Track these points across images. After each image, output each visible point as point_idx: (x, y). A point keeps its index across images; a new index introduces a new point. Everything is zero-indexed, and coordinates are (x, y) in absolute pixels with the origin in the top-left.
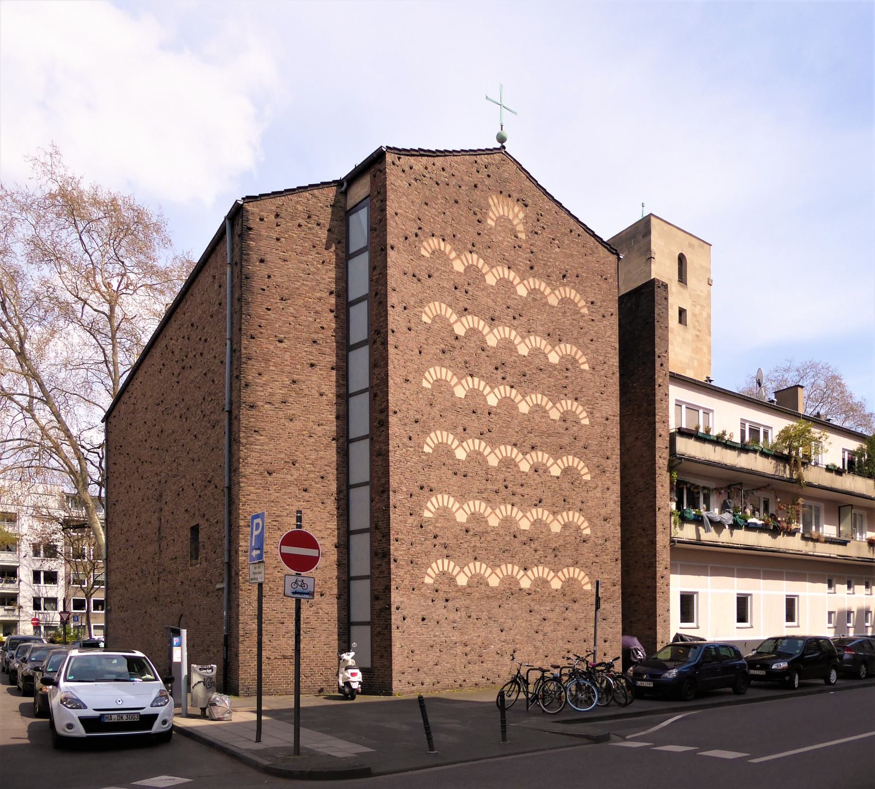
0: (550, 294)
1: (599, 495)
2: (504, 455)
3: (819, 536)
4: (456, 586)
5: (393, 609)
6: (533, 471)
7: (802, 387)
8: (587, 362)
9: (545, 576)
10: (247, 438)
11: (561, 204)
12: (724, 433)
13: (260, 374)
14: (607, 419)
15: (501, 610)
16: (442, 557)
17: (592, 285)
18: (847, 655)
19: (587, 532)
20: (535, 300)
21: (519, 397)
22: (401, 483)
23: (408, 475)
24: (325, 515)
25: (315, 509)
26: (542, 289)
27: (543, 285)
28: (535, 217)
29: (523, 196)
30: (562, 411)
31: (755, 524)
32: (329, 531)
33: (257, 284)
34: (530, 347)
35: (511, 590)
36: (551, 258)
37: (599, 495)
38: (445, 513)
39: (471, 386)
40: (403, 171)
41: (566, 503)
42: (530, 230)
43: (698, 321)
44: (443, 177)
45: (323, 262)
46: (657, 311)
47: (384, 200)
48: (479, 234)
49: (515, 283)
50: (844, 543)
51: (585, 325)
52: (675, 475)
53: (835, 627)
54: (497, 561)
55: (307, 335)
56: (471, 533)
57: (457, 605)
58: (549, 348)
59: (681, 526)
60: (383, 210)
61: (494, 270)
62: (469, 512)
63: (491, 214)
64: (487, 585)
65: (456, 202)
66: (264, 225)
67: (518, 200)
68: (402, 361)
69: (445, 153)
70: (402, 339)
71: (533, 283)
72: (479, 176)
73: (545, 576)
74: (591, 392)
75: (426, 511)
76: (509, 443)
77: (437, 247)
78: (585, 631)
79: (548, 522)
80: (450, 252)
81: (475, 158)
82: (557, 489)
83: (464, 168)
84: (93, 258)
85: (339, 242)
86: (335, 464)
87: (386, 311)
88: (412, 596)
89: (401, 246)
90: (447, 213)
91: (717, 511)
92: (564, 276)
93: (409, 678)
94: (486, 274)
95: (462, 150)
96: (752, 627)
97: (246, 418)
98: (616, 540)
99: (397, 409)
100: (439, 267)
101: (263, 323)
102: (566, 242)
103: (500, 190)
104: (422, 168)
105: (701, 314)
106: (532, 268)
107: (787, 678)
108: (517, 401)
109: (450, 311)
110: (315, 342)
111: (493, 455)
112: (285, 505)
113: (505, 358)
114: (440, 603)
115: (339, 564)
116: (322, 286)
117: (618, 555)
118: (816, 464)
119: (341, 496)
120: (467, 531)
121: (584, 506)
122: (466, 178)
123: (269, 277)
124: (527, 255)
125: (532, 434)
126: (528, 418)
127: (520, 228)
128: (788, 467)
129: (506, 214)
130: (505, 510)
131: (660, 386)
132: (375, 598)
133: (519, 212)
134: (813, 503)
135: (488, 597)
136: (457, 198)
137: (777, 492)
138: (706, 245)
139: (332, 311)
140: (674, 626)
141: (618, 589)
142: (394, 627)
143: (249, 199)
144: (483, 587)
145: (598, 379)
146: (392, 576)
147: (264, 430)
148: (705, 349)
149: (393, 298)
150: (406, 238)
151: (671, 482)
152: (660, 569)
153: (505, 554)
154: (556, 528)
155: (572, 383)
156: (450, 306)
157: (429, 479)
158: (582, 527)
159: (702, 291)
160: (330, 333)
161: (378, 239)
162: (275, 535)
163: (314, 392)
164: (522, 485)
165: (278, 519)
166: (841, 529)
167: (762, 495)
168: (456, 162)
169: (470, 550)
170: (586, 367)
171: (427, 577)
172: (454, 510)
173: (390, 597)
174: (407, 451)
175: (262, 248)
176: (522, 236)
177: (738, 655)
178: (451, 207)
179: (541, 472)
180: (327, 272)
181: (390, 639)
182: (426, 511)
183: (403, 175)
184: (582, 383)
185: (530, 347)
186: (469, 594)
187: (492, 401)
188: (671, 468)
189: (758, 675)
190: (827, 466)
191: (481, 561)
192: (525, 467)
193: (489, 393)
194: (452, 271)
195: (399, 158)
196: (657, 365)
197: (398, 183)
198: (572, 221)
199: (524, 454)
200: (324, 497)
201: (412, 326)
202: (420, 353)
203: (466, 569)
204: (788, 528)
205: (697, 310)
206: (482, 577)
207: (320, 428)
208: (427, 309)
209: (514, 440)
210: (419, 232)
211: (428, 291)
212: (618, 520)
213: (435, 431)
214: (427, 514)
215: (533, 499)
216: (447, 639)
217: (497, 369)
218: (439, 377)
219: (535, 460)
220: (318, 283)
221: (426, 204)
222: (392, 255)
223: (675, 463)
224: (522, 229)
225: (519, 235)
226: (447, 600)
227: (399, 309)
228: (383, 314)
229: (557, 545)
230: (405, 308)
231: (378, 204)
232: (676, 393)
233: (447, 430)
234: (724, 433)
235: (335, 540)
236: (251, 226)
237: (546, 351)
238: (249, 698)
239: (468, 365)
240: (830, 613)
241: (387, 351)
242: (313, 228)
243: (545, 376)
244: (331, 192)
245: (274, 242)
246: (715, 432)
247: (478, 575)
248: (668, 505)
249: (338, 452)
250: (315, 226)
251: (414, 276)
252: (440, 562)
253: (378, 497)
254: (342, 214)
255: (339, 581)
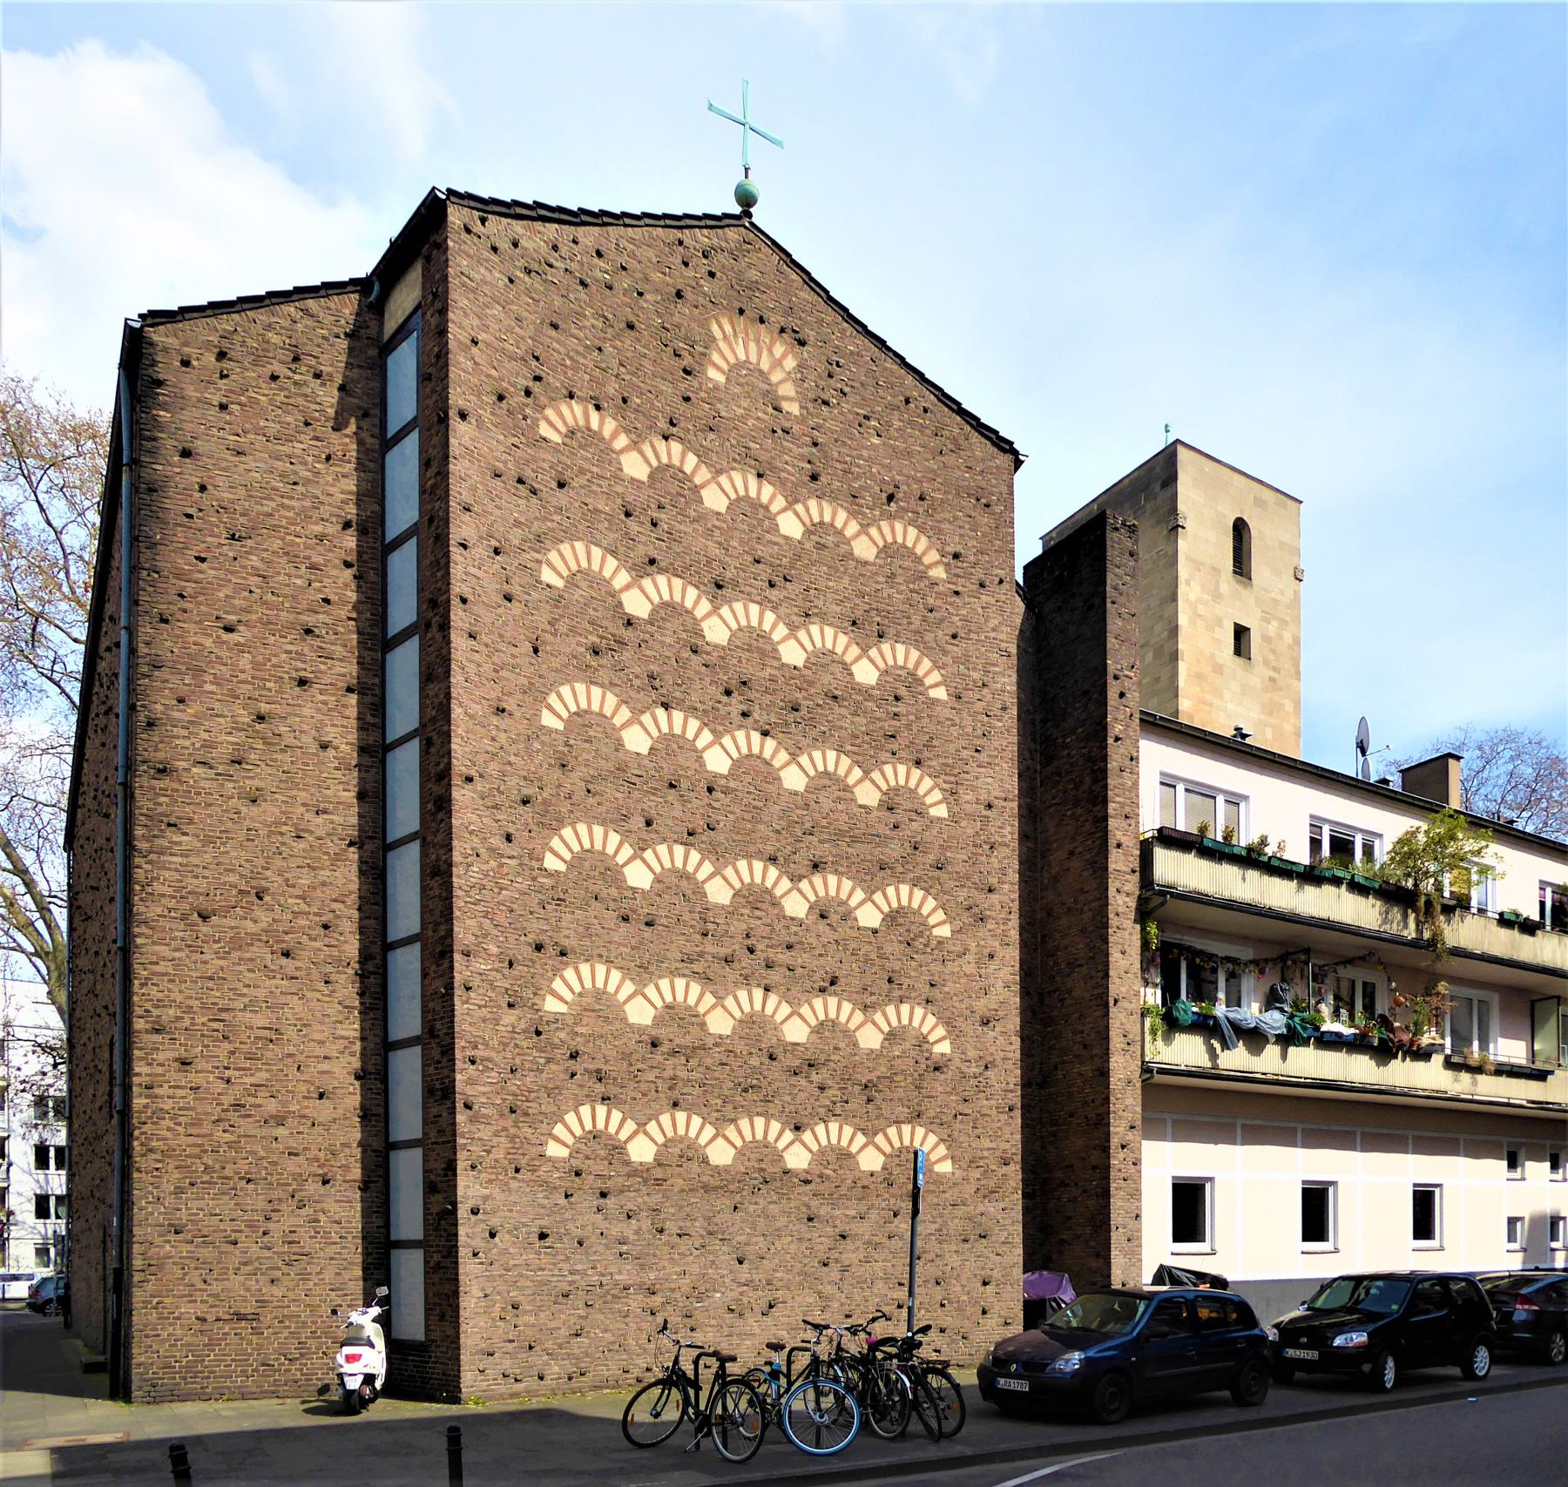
0: (857, 535)
1: (970, 969)
2: (747, 880)
3: (1484, 1061)
4: (628, 1163)
5: (463, 1212)
6: (814, 917)
7: (1458, 758)
8: (944, 683)
9: (844, 1143)
10: (150, 838)
11: (883, 342)
12: (1264, 842)
13: (181, 701)
14: (990, 806)
15: (738, 1216)
16: (590, 1099)
17: (956, 518)
18: (1521, 1312)
19: (944, 1048)
20: (821, 546)
21: (783, 756)
22: (485, 936)
23: (502, 918)
24: (333, 1010)
25: (309, 995)
26: (839, 524)
27: (842, 516)
28: (822, 368)
29: (794, 323)
30: (884, 787)
31: (1338, 1035)
32: (341, 1044)
33: (173, 505)
34: (810, 648)
35: (762, 1171)
36: (860, 457)
37: (970, 969)
38: (597, 1005)
39: (665, 729)
40: (495, 249)
41: (894, 986)
42: (811, 395)
43: (1273, 651)
44: (600, 271)
45: (328, 458)
46: (1110, 579)
47: (443, 311)
48: (687, 399)
49: (774, 508)
50: (1541, 1076)
51: (939, 603)
52: (1153, 929)
53: (1524, 1250)
54: (729, 1111)
55: (291, 617)
56: (664, 1048)
57: (630, 1206)
58: (855, 651)
59: (1168, 1038)
60: (442, 332)
61: (723, 479)
62: (659, 1004)
63: (716, 357)
64: (705, 1161)
65: (631, 326)
66: (190, 375)
67: (782, 330)
68: (487, 668)
69: (603, 218)
70: (487, 617)
71: (817, 510)
72: (689, 273)
73: (844, 1143)
74: (952, 748)
75: (549, 998)
76: (758, 855)
77: (582, 423)
78: (938, 1262)
79: (852, 1026)
80: (615, 435)
81: (678, 234)
82: (873, 956)
83: (651, 254)
84: (64, 538)
85: (366, 415)
86: (354, 897)
87: (447, 555)
88: (514, 1185)
89: (486, 415)
90: (608, 348)
91: (1255, 1007)
92: (891, 498)
93: (506, 1364)
94: (703, 486)
95: (646, 215)
96: (1336, 1251)
97: (150, 796)
98: (1009, 1065)
99: (473, 773)
100: (586, 466)
101: (190, 588)
102: (897, 424)
103: (737, 305)
104: (545, 249)
105: (1280, 637)
106: (814, 477)
107: (1367, 1368)
108: (777, 763)
109: (612, 563)
110: (308, 631)
111: (718, 880)
112: (239, 985)
113: (750, 670)
114: (586, 1201)
115: (366, 1115)
116: (325, 511)
117: (1016, 1099)
118: (1482, 911)
119: (370, 967)
120: (654, 1045)
121: (936, 993)
122: (656, 276)
123: (203, 488)
124: (805, 450)
125: (815, 837)
126: (805, 800)
127: (787, 390)
128: (1412, 917)
129: (753, 359)
130: (749, 1000)
131: (1117, 739)
132: (430, 1188)
133: (784, 356)
134: (1474, 994)
135: (706, 1188)
136: (632, 318)
137: (1391, 969)
138: (1290, 502)
139: (348, 565)
140: (1148, 1249)
141: (1014, 1172)
142: (464, 1252)
143: (155, 317)
144: (695, 1167)
145: (968, 721)
146: (460, 1141)
147: (191, 821)
148: (1289, 706)
149: (461, 528)
150: (501, 398)
151: (1145, 944)
152: (1118, 1130)
153: (751, 1095)
154: (870, 1039)
155: (909, 727)
156: (614, 553)
157: (558, 929)
158: (931, 1039)
159: (1282, 593)
160: (344, 612)
161: (435, 397)
162: (217, 1051)
163: (307, 740)
164: (789, 947)
165: (224, 1016)
166: (1536, 1047)
167: (1359, 975)
168: (632, 240)
169: (661, 1086)
170: (940, 693)
171: (551, 1143)
172: (779, 1018)
173: (455, 1186)
174: (501, 865)
175: (186, 426)
176: (793, 408)
177: (1245, 1313)
178: (617, 336)
179: (834, 918)
180: (337, 479)
181: (455, 1280)
182: (549, 998)
183: (493, 257)
184: (932, 728)
185: (810, 648)
186: (659, 1182)
187: (717, 763)
188: (1144, 914)
189: (1304, 1360)
190: (1501, 914)
191: (690, 1110)
192: (796, 907)
193: (711, 745)
194: (618, 475)
195: (483, 220)
196: (1112, 694)
197: (480, 273)
198: (909, 380)
199: (795, 878)
200: (329, 969)
201: (516, 590)
202: (536, 651)
203: (652, 1127)
204: (1412, 1042)
205: (1272, 628)
206: (692, 1145)
207: (321, 819)
208: (553, 556)
209: (770, 849)
210: (536, 388)
211: (557, 518)
212: (1014, 1023)
213: (573, 825)
214: (551, 1005)
215: (817, 977)
216: (605, 1280)
217: (728, 693)
218: (584, 706)
219: (822, 893)
220: (317, 503)
221: (555, 326)
222: (461, 435)
223: (1152, 905)
224: (793, 394)
225: (785, 406)
226: (603, 1195)
227: (481, 551)
228: (443, 561)
229: (873, 1076)
230: (497, 552)
231: (434, 321)
232: (1156, 759)
233: (603, 823)
234: (1264, 842)
235: (356, 1063)
236: (161, 377)
237: (848, 659)
238: (154, 1407)
239: (657, 683)
240: (1512, 1222)
241: (449, 642)
242: (305, 383)
243: (843, 711)
244: (348, 306)
245: (214, 412)
246: (1245, 839)
247: (682, 1139)
248: (1137, 994)
249: (362, 872)
250: (309, 378)
251: (520, 481)
252: (585, 1111)
253: (433, 968)
254: (373, 352)
255: (364, 1152)
